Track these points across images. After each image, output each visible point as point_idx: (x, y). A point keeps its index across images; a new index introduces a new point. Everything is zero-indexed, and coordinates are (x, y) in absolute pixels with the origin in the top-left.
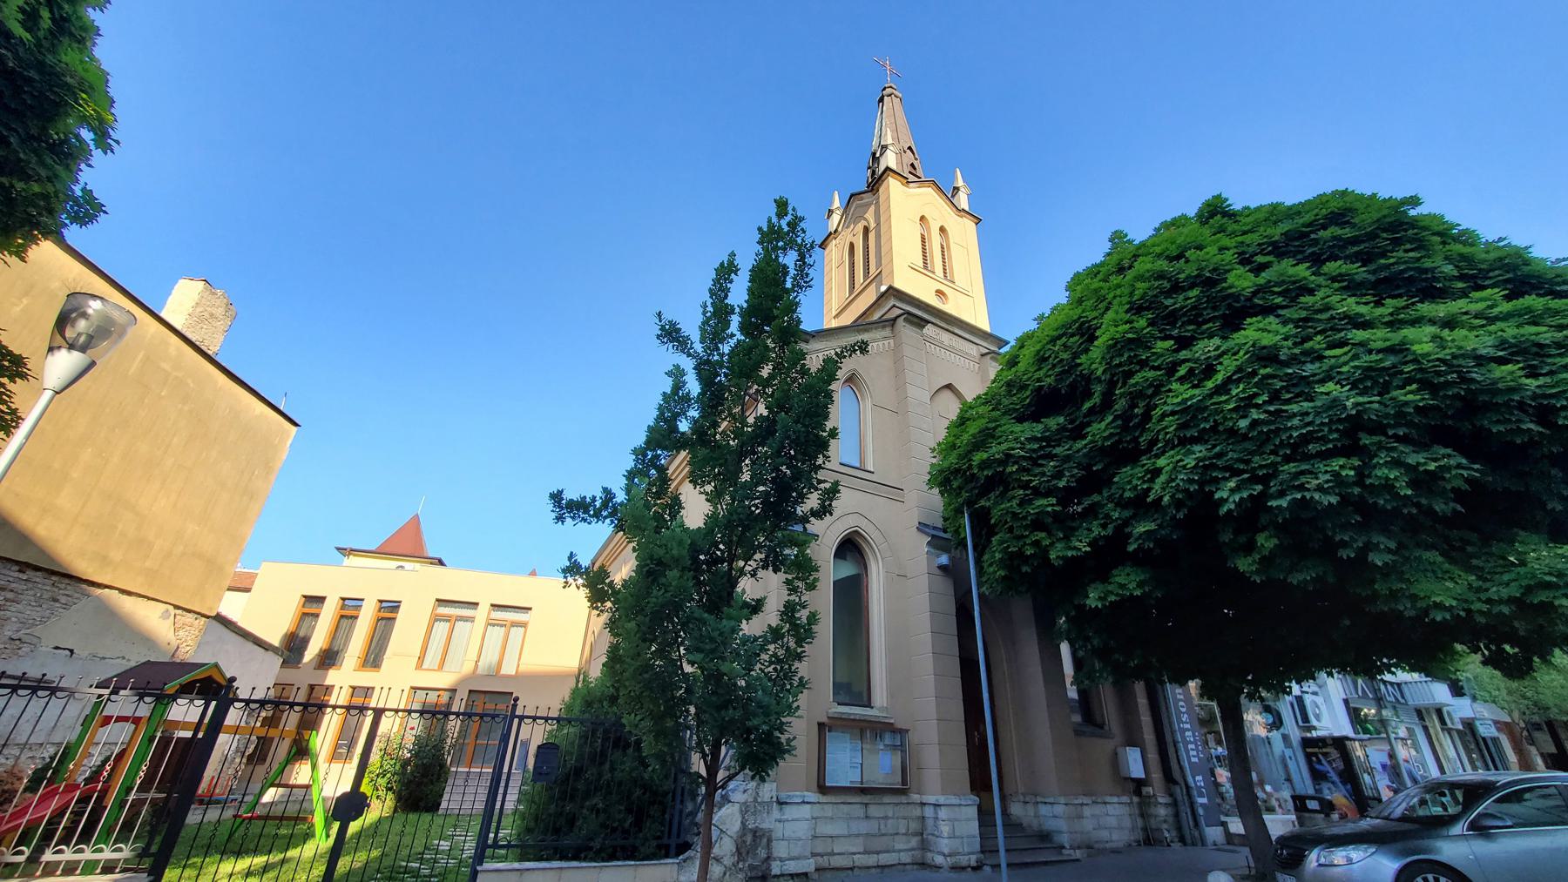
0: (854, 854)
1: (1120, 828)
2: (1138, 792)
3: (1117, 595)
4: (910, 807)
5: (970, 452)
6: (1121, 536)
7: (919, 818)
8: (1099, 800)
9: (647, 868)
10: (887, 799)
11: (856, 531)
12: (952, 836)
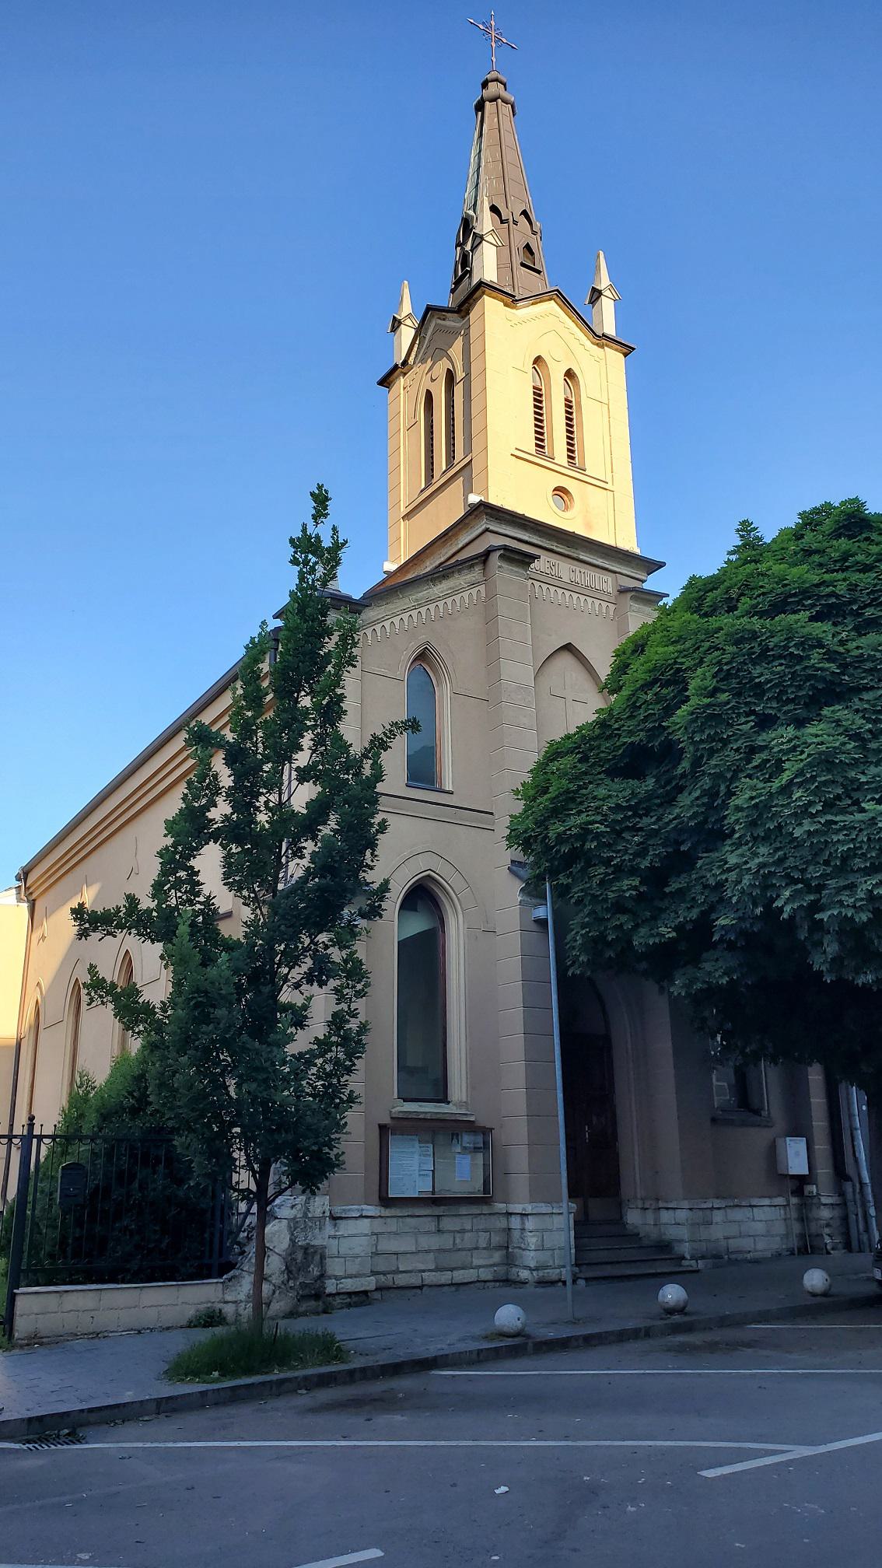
0: (424, 1271)
1: (768, 1234)
2: (799, 1192)
3: (705, 982)
4: (493, 1218)
5: (548, 818)
6: (704, 925)
7: (504, 1230)
8: (744, 1204)
9: (188, 1289)
10: (463, 1210)
11: (429, 876)
12: (541, 1248)
